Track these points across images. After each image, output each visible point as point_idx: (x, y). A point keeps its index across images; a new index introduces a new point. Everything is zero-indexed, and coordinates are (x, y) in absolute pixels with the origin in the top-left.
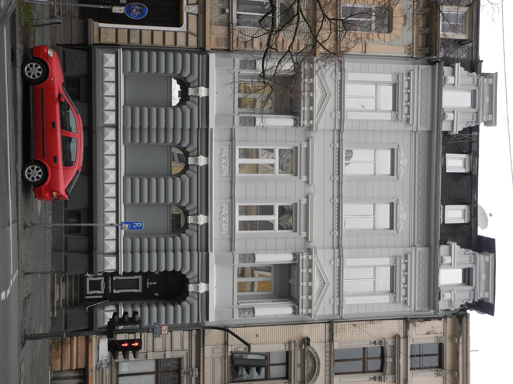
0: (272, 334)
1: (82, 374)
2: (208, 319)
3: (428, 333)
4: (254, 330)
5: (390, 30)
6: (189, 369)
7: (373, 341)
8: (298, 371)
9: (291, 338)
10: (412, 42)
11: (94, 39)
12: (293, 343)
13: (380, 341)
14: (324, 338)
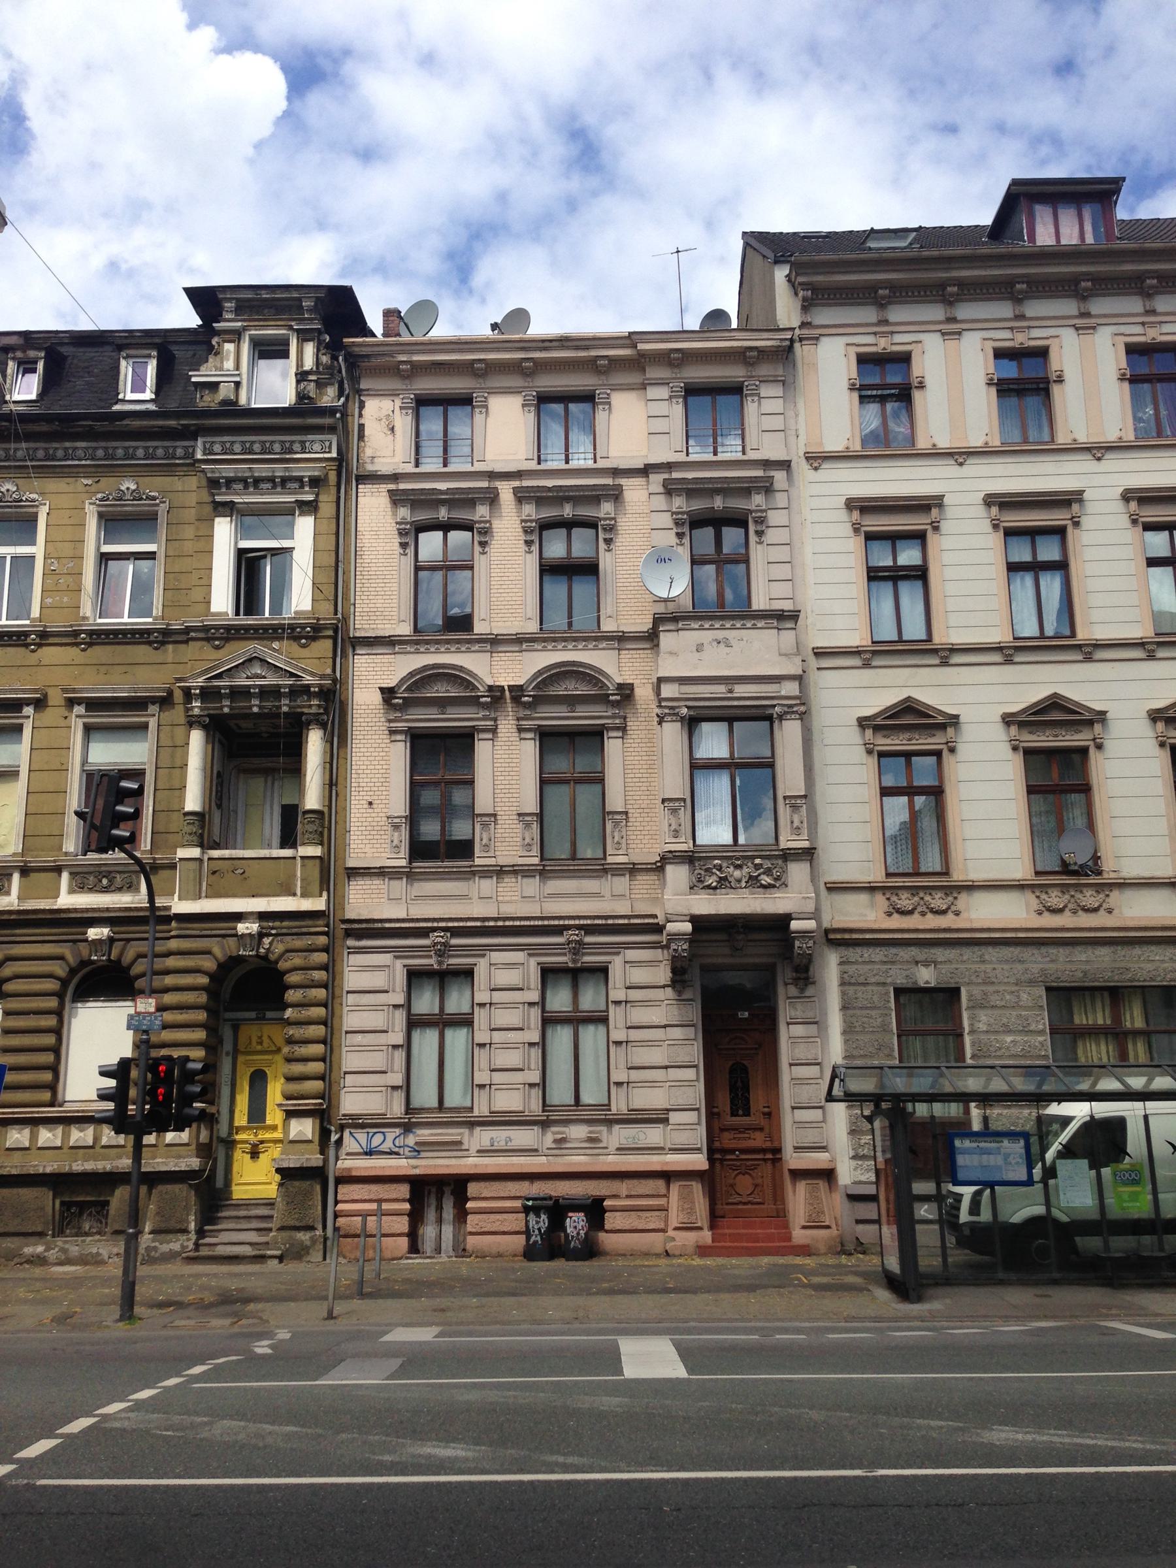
0: (369, 772)
1: (434, 1190)
3: (392, 429)
4: (356, 811)
6: (432, 953)
8: (582, 710)
9: (382, 728)
12: (392, 725)
13: (526, 531)
14: (386, 656)
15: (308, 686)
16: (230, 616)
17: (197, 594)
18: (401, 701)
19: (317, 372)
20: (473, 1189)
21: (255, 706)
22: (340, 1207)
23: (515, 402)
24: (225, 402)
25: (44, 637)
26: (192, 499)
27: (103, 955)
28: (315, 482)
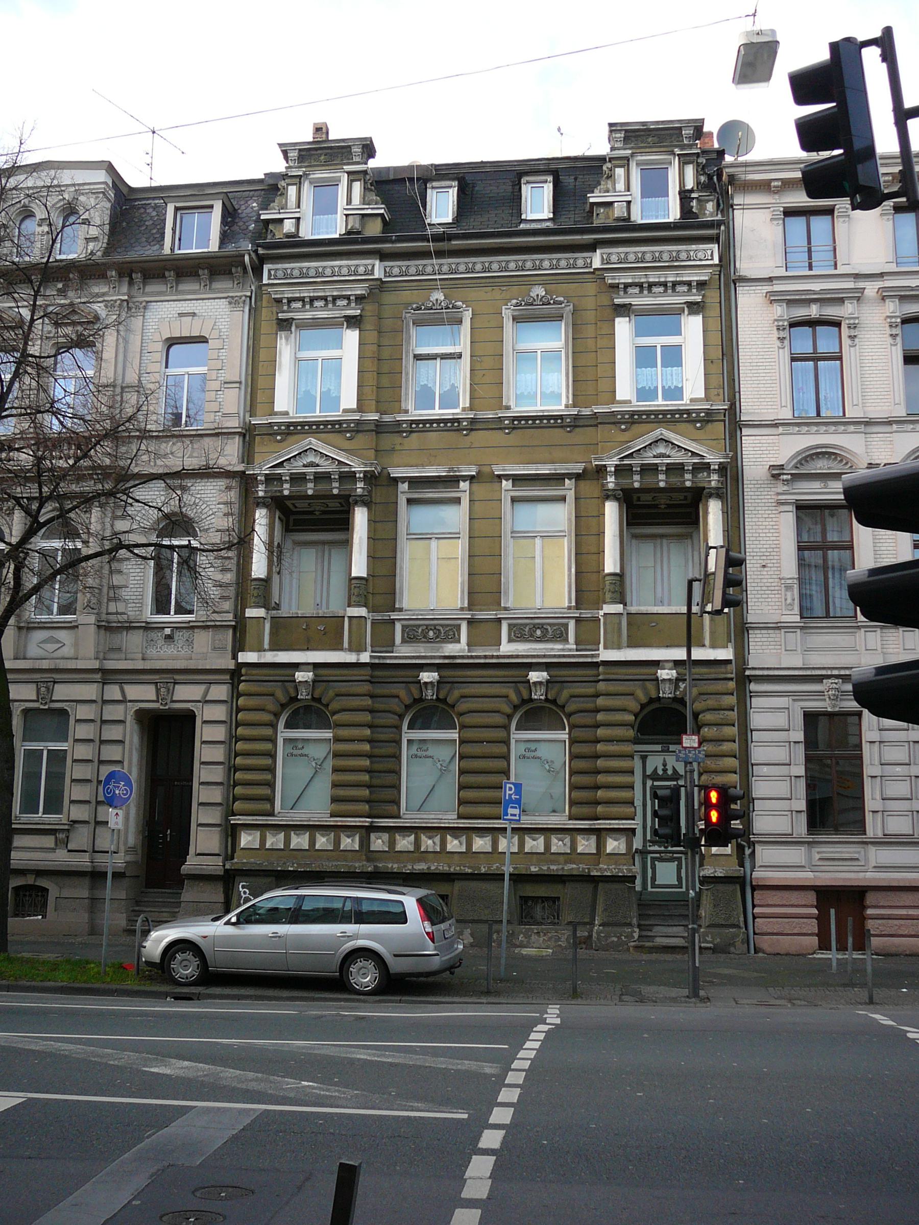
2: (728, 662)
5: (205, 340)
6: (826, 697)
7: (778, 343)
10: (224, 300)
11: (214, 865)
12: (780, 497)
15: (354, 472)
16: (291, 415)
17: (603, 385)
18: (789, 477)
19: (698, 190)
20: (870, 898)
21: (662, 481)
22: (757, 910)
23: (765, 215)
24: (288, 236)
25: (474, 425)
26: (590, 303)
27: (542, 695)
28: (701, 285)
